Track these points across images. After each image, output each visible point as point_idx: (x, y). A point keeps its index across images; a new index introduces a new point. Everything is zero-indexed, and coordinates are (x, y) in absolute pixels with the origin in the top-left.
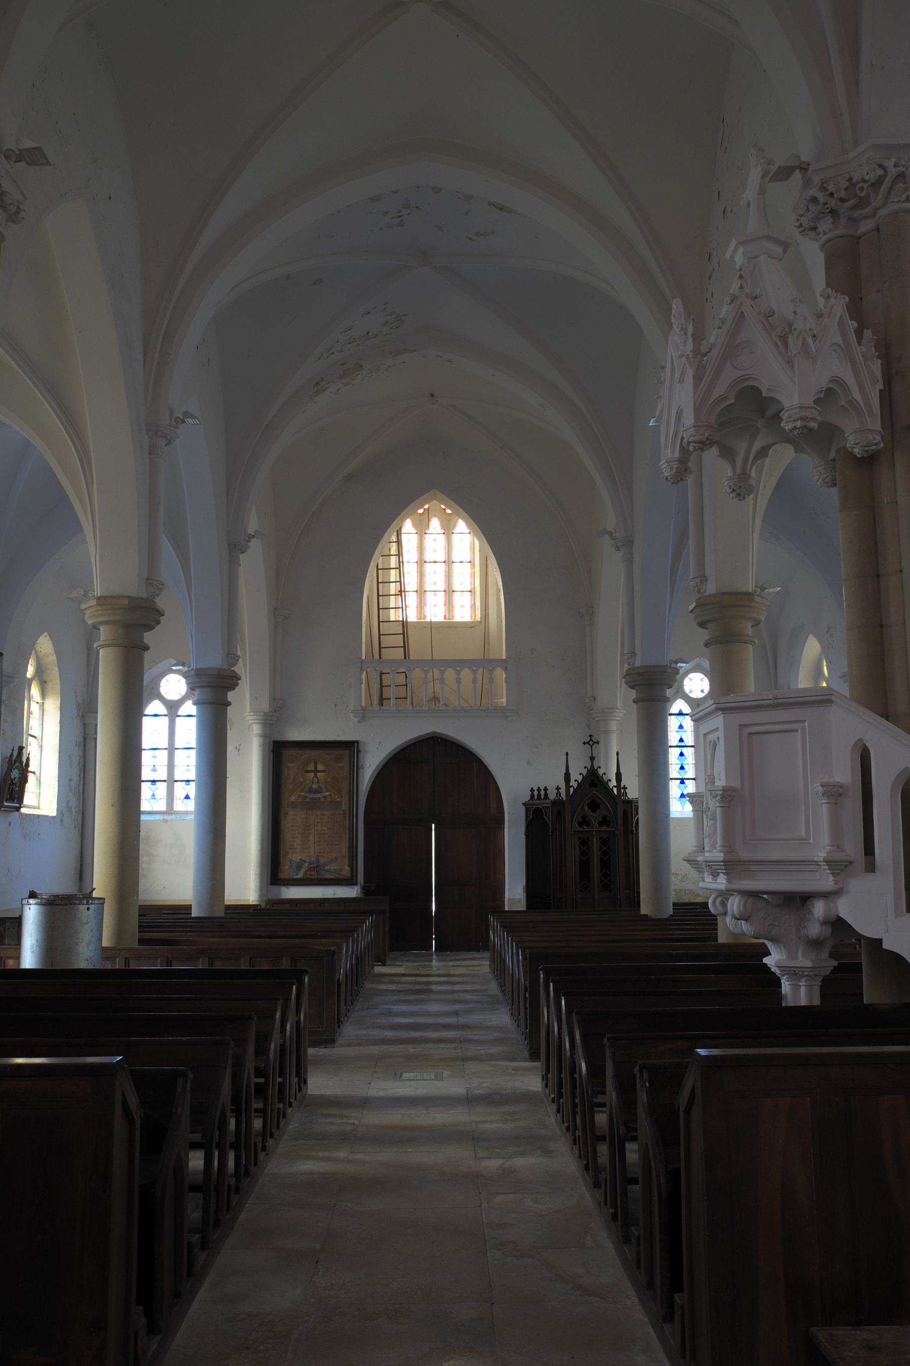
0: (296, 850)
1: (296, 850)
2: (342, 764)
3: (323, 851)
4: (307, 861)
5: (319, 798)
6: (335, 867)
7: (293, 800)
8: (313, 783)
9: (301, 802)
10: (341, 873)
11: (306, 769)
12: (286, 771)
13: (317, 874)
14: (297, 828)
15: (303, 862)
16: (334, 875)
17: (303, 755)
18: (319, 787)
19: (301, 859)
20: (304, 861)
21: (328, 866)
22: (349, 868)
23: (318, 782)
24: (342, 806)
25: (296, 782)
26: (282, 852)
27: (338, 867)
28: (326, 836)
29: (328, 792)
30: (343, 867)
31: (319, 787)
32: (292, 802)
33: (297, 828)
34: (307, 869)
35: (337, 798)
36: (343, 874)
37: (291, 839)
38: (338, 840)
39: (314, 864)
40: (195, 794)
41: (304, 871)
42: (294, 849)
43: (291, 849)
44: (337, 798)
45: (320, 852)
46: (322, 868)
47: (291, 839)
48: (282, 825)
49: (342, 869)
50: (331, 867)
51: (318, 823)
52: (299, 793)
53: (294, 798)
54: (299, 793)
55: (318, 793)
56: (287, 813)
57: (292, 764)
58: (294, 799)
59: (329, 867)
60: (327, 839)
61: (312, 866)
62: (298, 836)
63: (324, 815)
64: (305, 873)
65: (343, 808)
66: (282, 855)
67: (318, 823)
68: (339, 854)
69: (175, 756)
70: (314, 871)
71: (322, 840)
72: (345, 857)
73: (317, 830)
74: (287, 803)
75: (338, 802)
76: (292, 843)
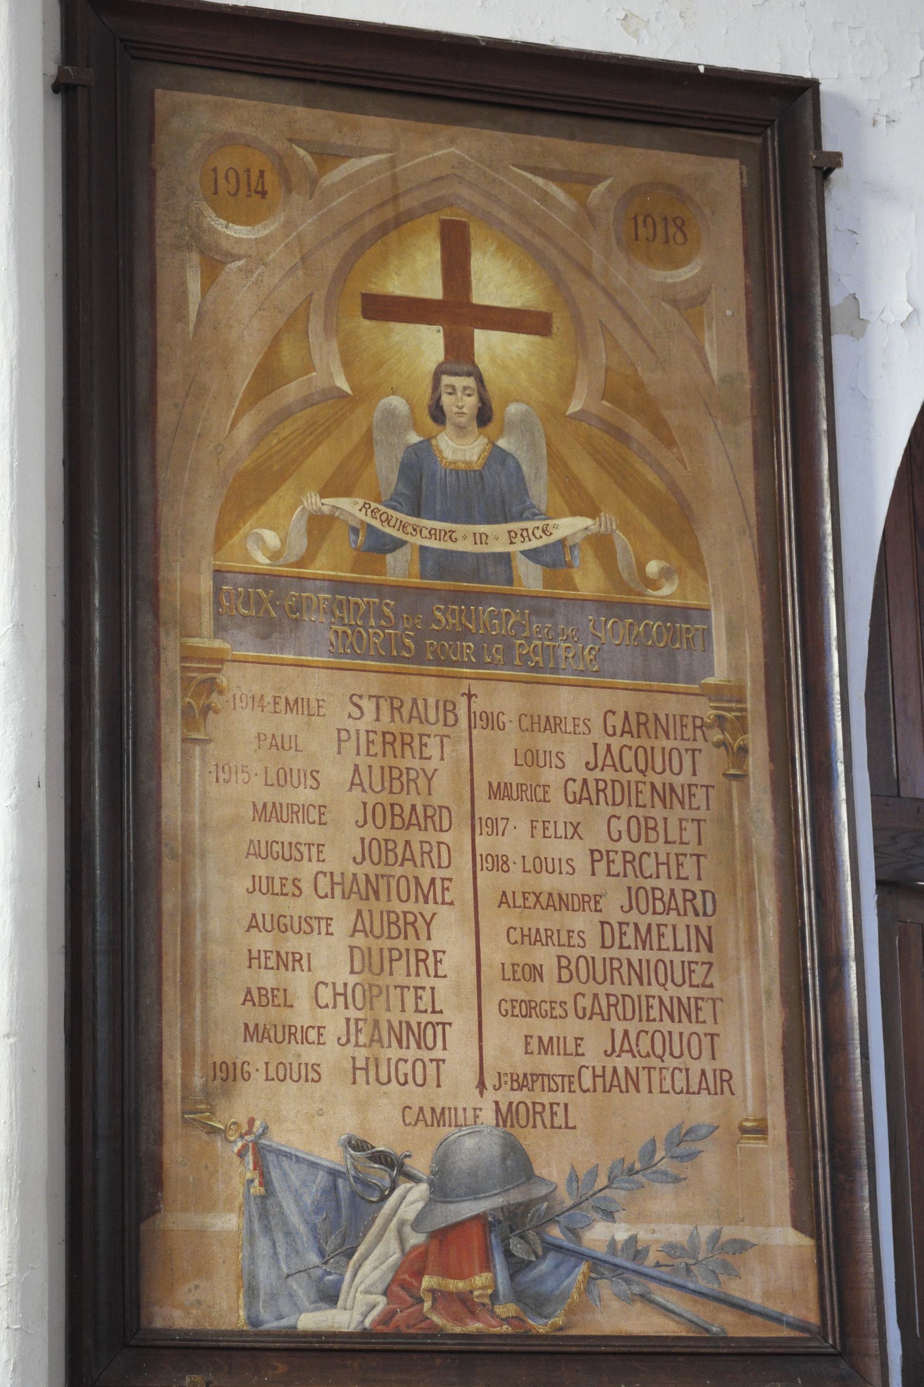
0: (310, 1054)
1: (310, 1054)
2: (686, 273)
3: (554, 1064)
4: (421, 1164)
5: (505, 559)
6: (677, 1233)
7: (262, 560)
8: (438, 414)
9: (338, 585)
10: (735, 1290)
11: (375, 288)
12: (194, 285)
13: (519, 1296)
14: (304, 832)
15: (380, 1175)
16: (667, 1311)
17: (342, 156)
18: (497, 457)
19: (356, 1145)
20: (383, 1159)
21: (609, 1215)
22: (807, 1242)
23: (484, 416)
24: (707, 646)
25: (292, 391)
26: (173, 1070)
27: (705, 1232)
28: (581, 921)
29: (575, 512)
30: (745, 1233)
31: (497, 457)
32: (265, 579)
33: (304, 832)
34: (415, 1239)
35: (666, 574)
36: (756, 1298)
37: (262, 941)
38: (688, 967)
39: (474, 1193)
40: (65, 517)
41: (395, 1257)
42: (290, 1033)
43: (252, 1033)
44: (666, 574)
45: (522, 1082)
46: (556, 1233)
47: (262, 941)
48: (171, 792)
49: (741, 1246)
50: (644, 1236)
51: (499, 791)
52: (313, 501)
53: (271, 538)
54: (313, 501)
55: (490, 520)
56: (211, 686)
57: (249, 220)
58: (275, 556)
59: (621, 1233)
60: (593, 949)
61: (468, 1209)
62: (321, 907)
63: (552, 724)
64: (301, 1287)
65: (719, 675)
66: (173, 1106)
67: (499, 791)
68: (704, 1100)
69: (60, 212)
70: (487, 1265)
71: (545, 956)
72: (761, 1130)
73: (500, 863)
74: (206, 584)
75: (668, 612)
76: (268, 980)
